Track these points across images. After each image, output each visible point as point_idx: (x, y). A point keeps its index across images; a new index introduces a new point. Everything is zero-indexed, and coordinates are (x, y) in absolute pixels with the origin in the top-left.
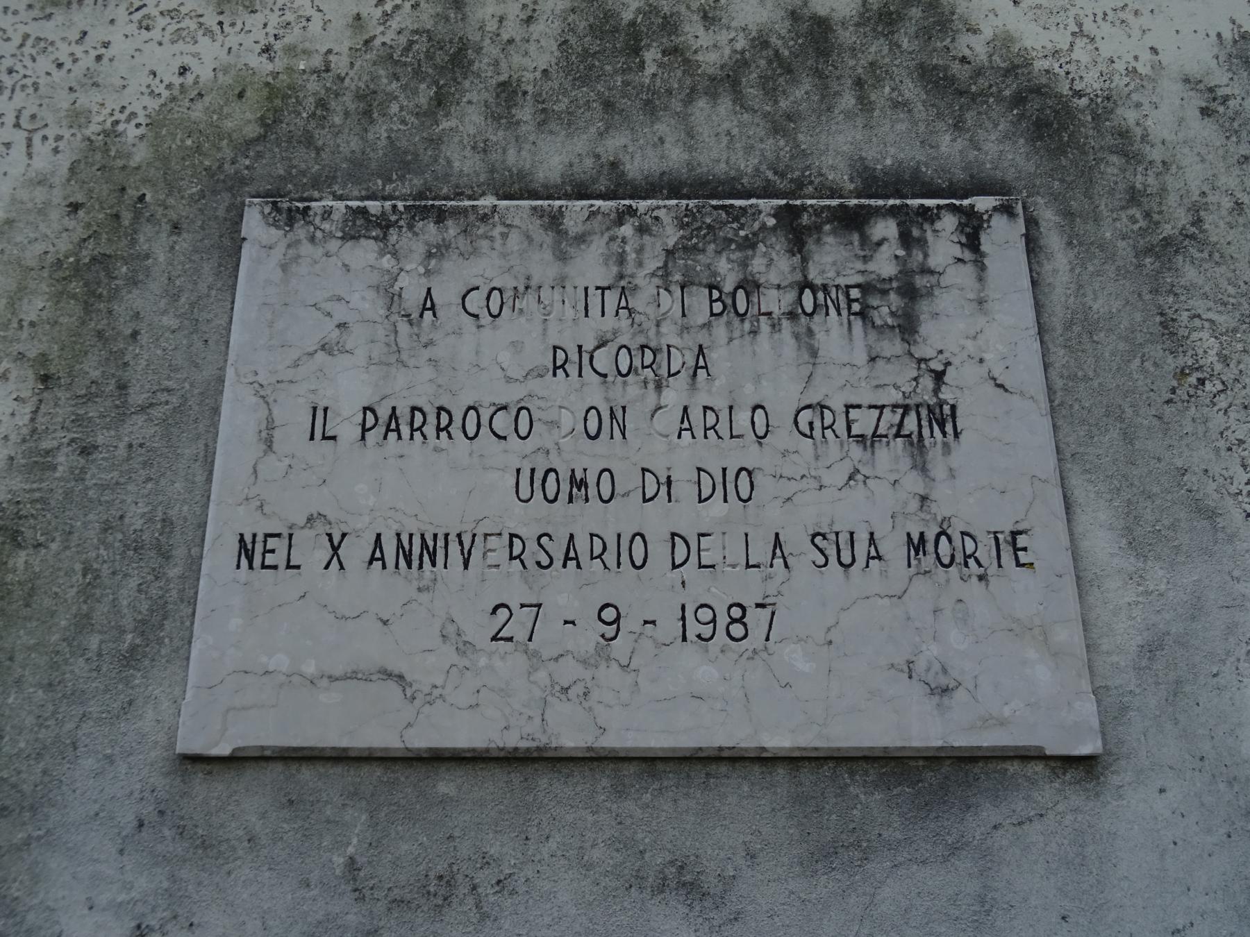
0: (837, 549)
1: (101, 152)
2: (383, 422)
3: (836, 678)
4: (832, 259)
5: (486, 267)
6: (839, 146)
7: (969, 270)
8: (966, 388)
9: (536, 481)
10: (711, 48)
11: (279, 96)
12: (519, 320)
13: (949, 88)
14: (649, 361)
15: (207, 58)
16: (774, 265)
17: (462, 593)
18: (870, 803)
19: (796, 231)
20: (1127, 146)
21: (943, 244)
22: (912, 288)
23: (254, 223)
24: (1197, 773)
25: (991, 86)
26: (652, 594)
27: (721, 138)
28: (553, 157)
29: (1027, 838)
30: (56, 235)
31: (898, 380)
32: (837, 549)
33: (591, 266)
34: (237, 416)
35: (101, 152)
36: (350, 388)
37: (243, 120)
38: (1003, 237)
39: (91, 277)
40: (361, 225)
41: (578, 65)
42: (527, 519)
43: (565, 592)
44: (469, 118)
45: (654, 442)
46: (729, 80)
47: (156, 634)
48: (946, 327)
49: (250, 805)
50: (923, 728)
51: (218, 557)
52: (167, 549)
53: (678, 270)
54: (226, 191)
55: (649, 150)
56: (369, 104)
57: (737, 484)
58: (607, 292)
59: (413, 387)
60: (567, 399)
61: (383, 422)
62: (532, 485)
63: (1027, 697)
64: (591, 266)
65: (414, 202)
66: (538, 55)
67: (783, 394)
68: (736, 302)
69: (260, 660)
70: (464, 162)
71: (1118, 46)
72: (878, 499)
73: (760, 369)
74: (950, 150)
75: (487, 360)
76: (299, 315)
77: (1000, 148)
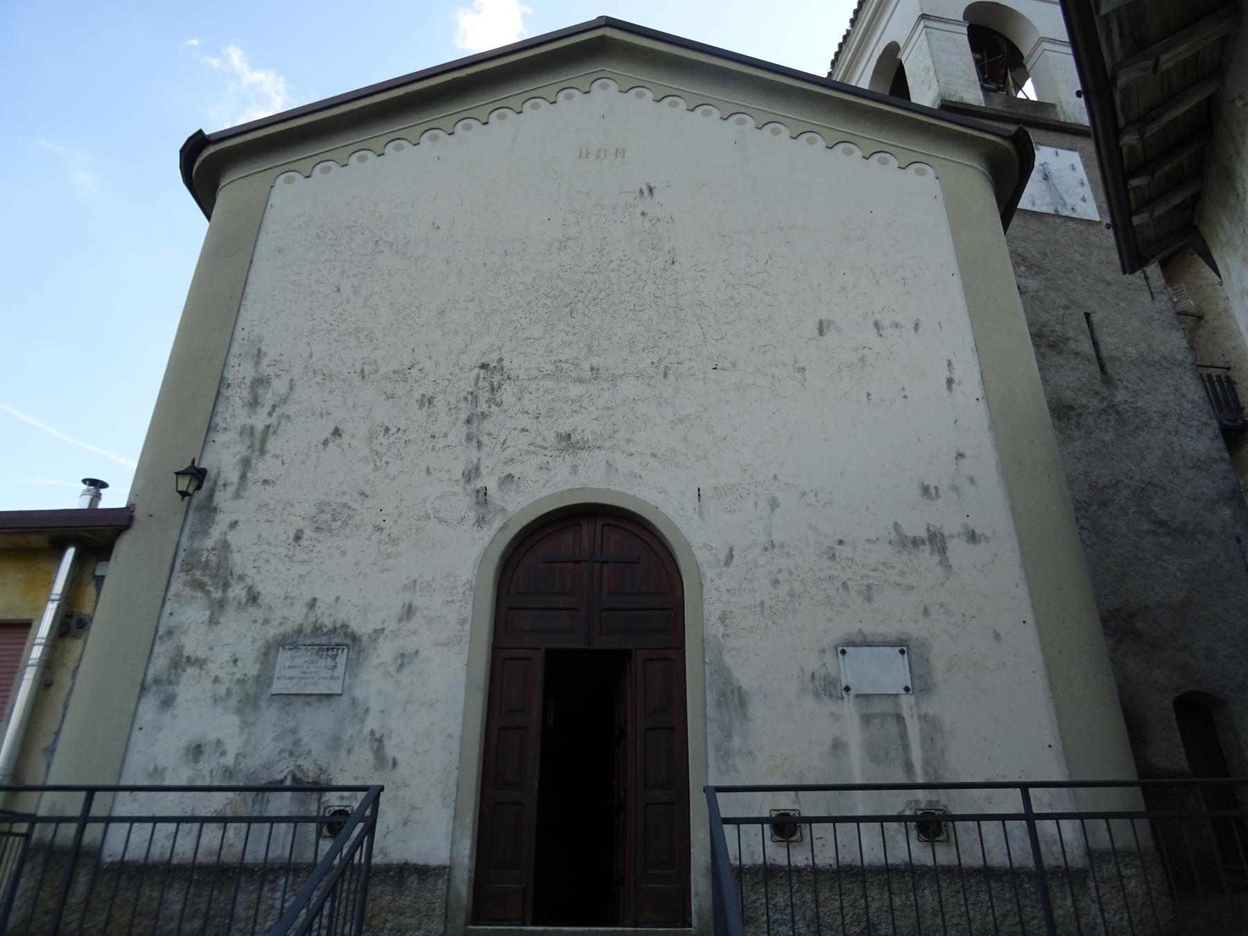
4: (330, 653)
6: (335, 641)
7: (230, 376)
10: (325, 630)
11: (284, 636)
12: (302, 658)
13: (346, 635)
15: (278, 631)
17: (294, 681)
24: (403, 428)
27: (324, 640)
28: (308, 642)
29: (334, 700)
30: (263, 650)
35: (267, 642)
36: (287, 664)
39: (266, 654)
41: (312, 632)
45: (312, 669)
47: (270, 685)
48: (338, 659)
55: (317, 641)
60: (305, 665)
62: (81, 655)
63: (336, 689)
65: (295, 647)
66: (308, 631)
68: (321, 657)
69: (278, 687)
72: (328, 674)
73: (322, 663)
74: (344, 641)
75: (299, 661)
77: (349, 641)
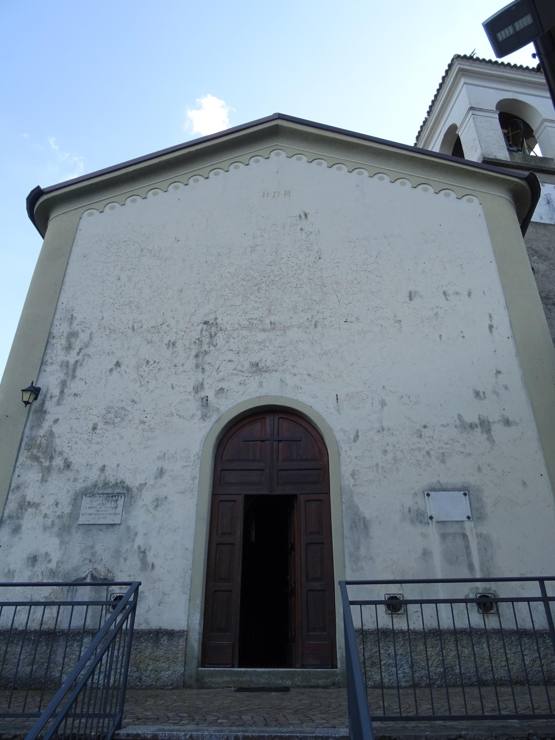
0: (110, 514)
1: (76, 492)
2: (89, 508)
3: (108, 521)
5: (96, 499)
8: (119, 506)
9: (96, 511)
11: (86, 488)
12: (97, 502)
14: (103, 504)
15: (82, 485)
16: (111, 499)
17: (92, 516)
18: (110, 526)
19: (112, 497)
20: (132, 491)
21: (120, 497)
22: (117, 500)
23: (84, 496)
25: (129, 279)
26: (101, 516)
27: (110, 491)
28: (100, 492)
31: (116, 505)
32: (110, 514)
33: (101, 499)
34: (82, 507)
35: (76, 492)
36: (88, 506)
37: (84, 490)
38: (123, 497)
39: (75, 500)
40: (90, 496)
41: (103, 486)
42: (96, 513)
43: (97, 516)
44: (96, 490)
45: (103, 509)
46: (111, 487)
47: (78, 519)
49: (81, 526)
50: (112, 523)
51: (81, 514)
52: (78, 514)
53: (106, 499)
54: (83, 494)
55: (106, 492)
56: (91, 489)
57: (106, 511)
58: (61, 607)
59: (91, 506)
60: (99, 506)
61: (89, 508)
64: (101, 499)
65: (93, 495)
66: (101, 485)
67: (109, 506)
68: (108, 501)
70: (96, 492)
71: (134, 485)
73: (109, 505)
74: (122, 491)
75: (95, 504)
76: (86, 501)
77: (125, 491)
